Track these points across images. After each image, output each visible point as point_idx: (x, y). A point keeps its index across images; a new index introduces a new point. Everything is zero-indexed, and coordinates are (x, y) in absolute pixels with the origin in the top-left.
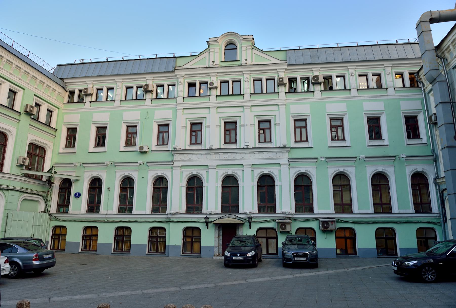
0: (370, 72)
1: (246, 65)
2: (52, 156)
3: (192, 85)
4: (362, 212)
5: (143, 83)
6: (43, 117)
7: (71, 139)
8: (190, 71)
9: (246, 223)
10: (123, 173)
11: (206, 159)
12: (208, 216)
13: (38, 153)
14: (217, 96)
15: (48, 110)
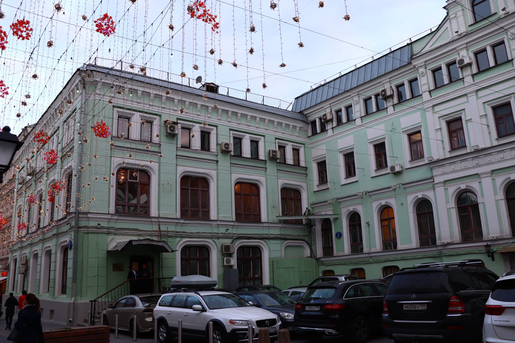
0: (442, 63)
3: (436, 71)
5: (379, 90)
7: (322, 174)
8: (477, 34)
10: (379, 202)
11: (441, 173)
12: (489, 243)
14: (473, 76)
15: (294, 149)
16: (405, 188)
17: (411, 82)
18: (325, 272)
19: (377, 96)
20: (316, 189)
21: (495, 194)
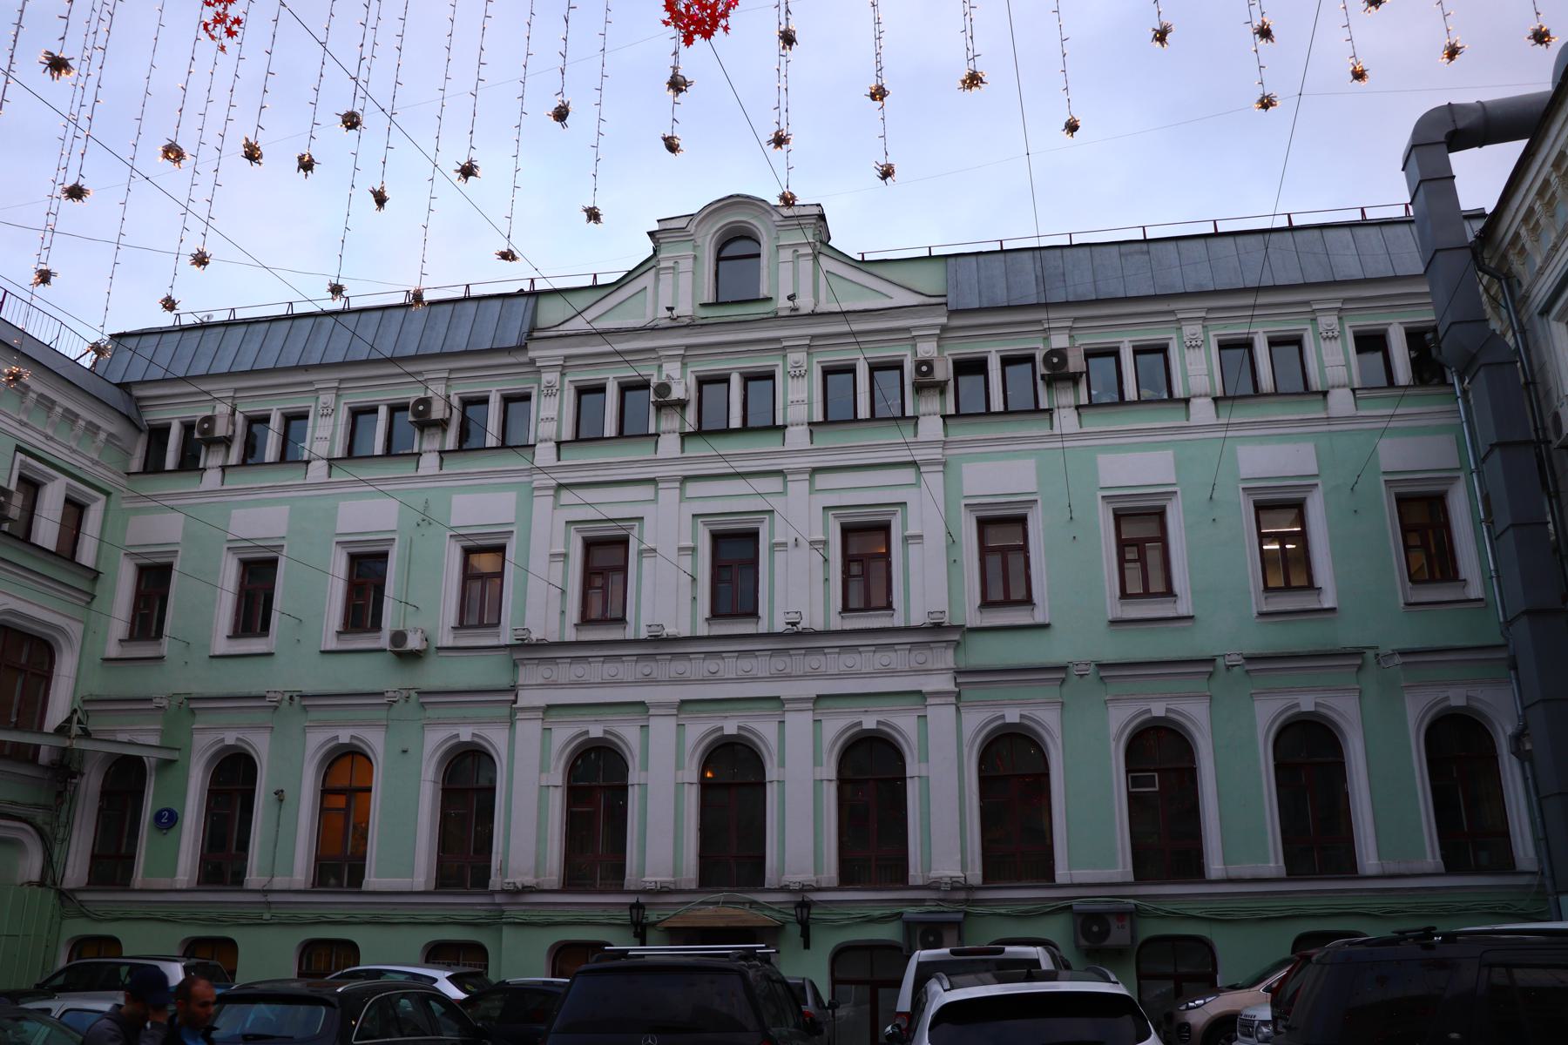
0: (1126, 339)
1: (795, 316)
2: (79, 669)
4: (1235, 871)
5: (412, 394)
6: (47, 532)
9: (788, 927)
13: (23, 660)
15: (69, 501)
16: (423, 704)
17: (508, 400)
18: (81, 945)
19: (395, 409)
20: (113, 651)
21: (679, 766)
